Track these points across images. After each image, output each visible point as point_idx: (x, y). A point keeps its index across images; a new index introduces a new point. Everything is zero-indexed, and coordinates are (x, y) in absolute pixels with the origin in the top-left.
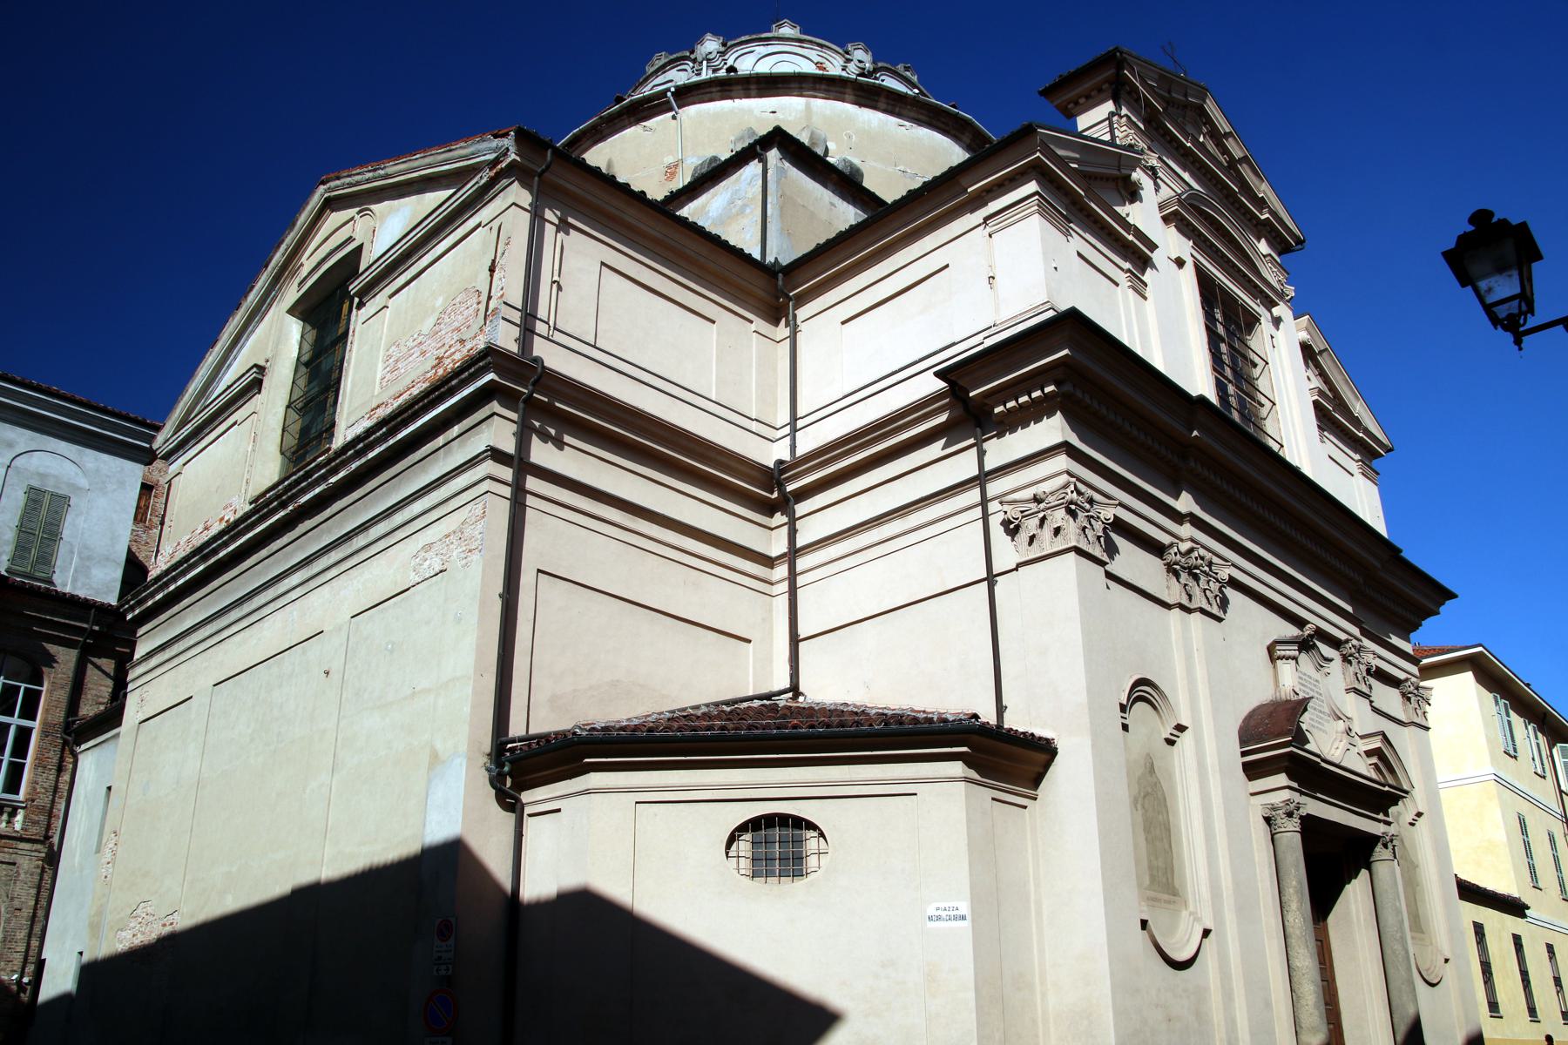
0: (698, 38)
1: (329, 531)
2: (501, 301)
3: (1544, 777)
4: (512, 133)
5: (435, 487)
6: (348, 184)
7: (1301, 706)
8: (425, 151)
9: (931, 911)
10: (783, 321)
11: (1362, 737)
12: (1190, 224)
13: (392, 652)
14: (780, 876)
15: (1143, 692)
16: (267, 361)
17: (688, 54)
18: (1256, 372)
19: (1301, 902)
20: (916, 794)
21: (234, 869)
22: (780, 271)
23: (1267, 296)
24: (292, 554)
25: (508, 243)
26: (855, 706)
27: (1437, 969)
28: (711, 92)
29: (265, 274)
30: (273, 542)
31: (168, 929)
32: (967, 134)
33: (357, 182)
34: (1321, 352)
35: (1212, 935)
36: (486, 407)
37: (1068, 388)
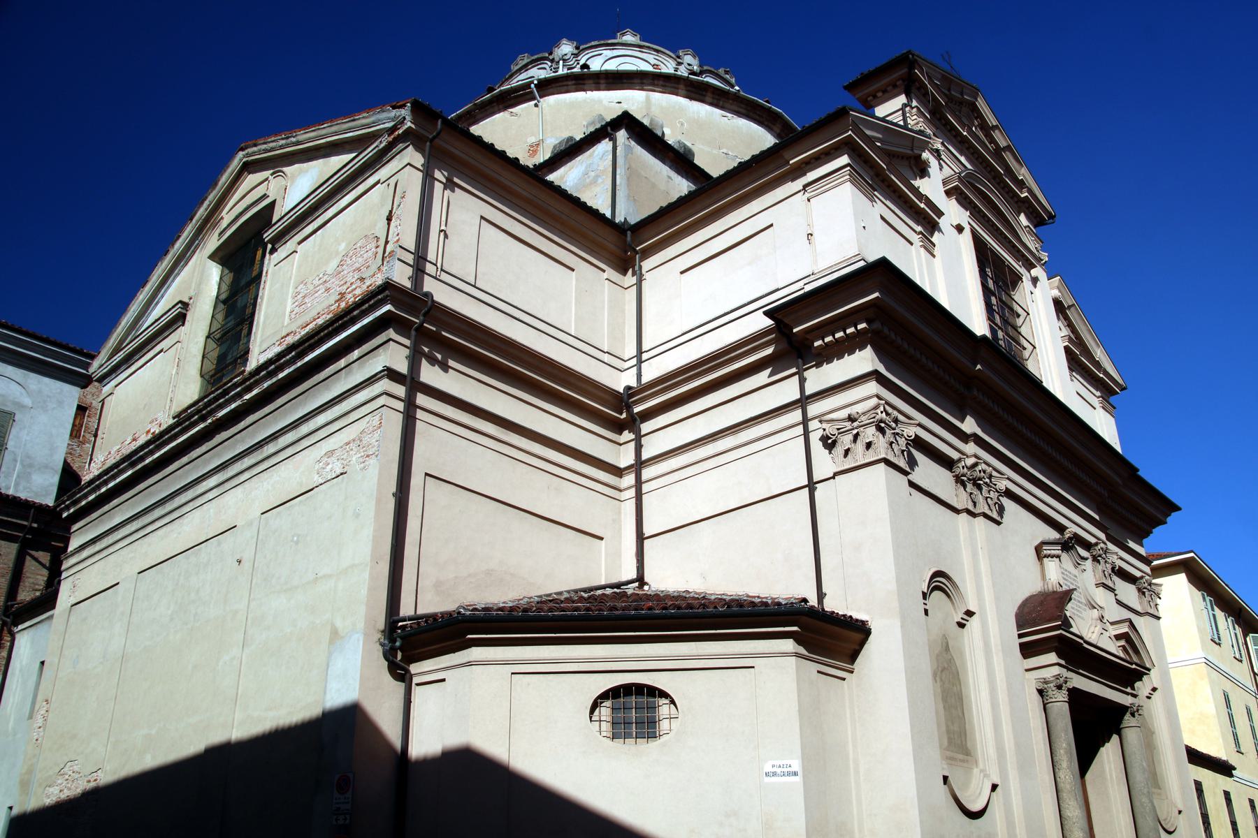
0: (556, 43)
1: (243, 441)
2: (397, 245)
3: (1241, 661)
4: (409, 105)
5: (338, 402)
6: (263, 150)
7: (1066, 596)
8: (331, 121)
9: (768, 768)
10: (630, 271)
11: (1112, 624)
12: (967, 197)
13: (297, 543)
14: (636, 738)
15: (940, 583)
16: (191, 299)
17: (547, 55)
18: (1019, 321)
19: (1070, 761)
20: (753, 667)
21: (153, 732)
22: (629, 229)
23: (1028, 260)
24: (209, 461)
25: (403, 197)
26: (696, 593)
27: (1172, 819)
28: (567, 85)
29: (190, 225)
30: (193, 450)
31: (92, 784)
32: (778, 125)
33: (272, 148)
34: (1069, 307)
35: (998, 789)
36: (384, 333)
37: (876, 325)
